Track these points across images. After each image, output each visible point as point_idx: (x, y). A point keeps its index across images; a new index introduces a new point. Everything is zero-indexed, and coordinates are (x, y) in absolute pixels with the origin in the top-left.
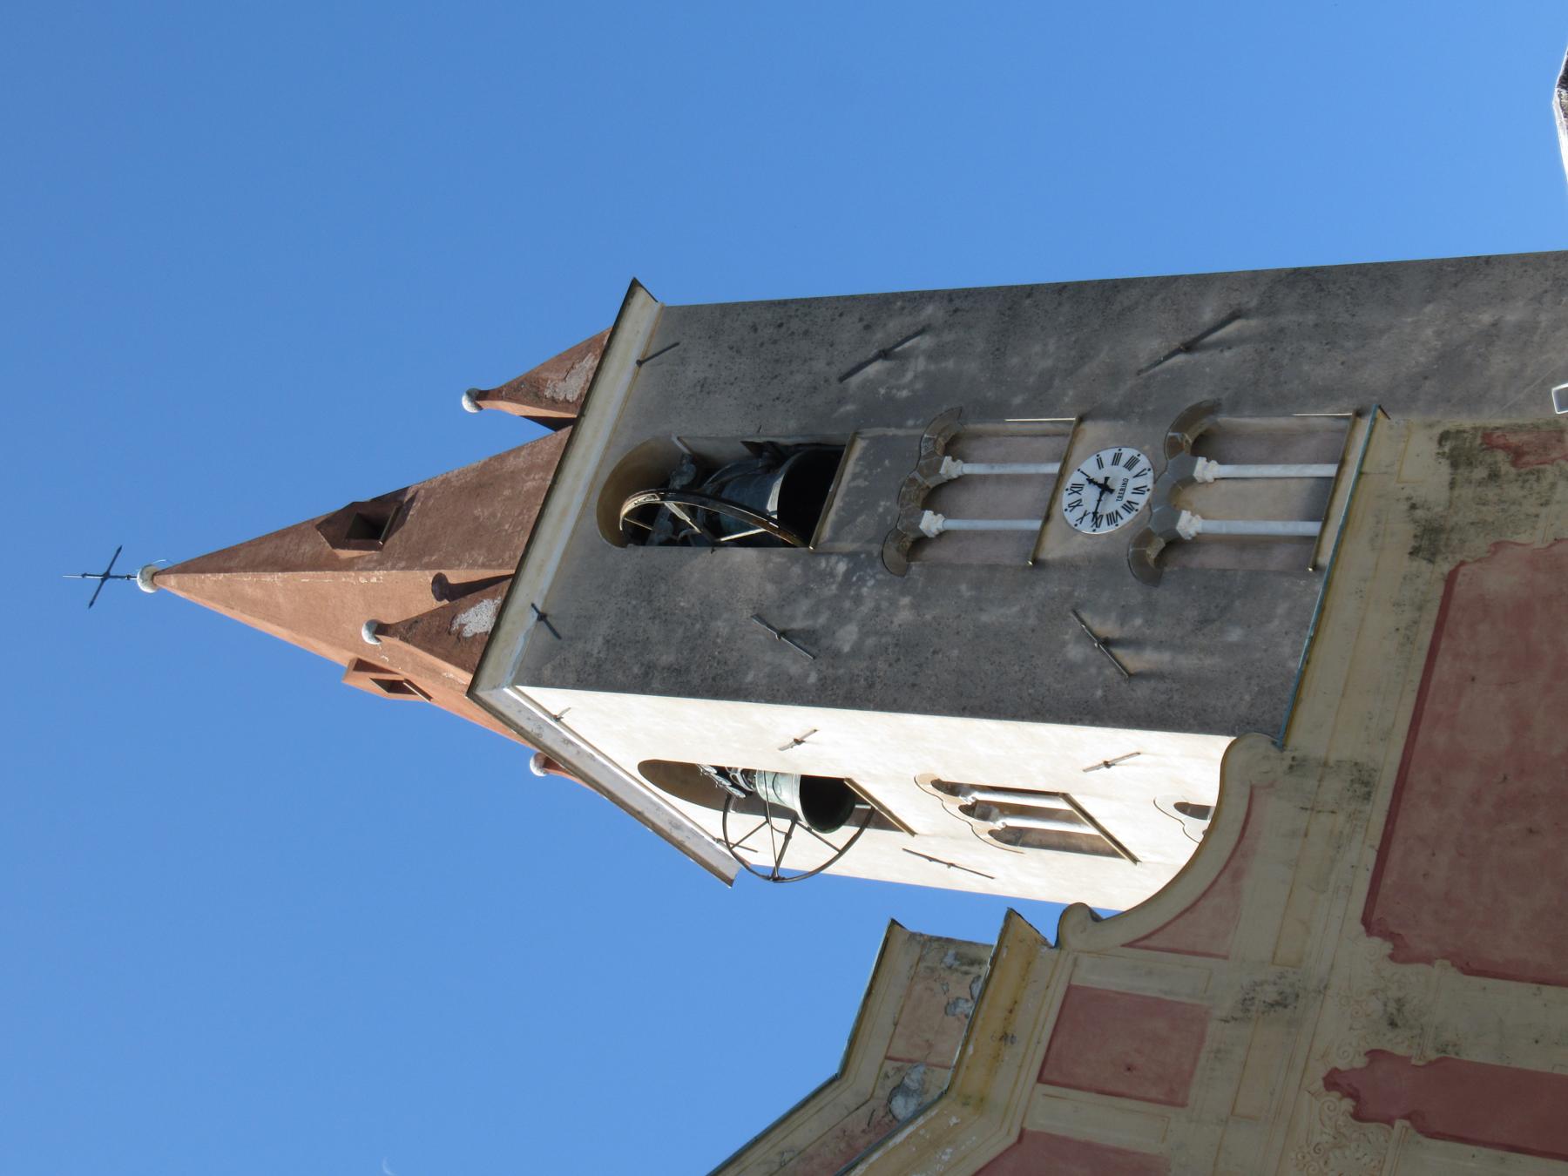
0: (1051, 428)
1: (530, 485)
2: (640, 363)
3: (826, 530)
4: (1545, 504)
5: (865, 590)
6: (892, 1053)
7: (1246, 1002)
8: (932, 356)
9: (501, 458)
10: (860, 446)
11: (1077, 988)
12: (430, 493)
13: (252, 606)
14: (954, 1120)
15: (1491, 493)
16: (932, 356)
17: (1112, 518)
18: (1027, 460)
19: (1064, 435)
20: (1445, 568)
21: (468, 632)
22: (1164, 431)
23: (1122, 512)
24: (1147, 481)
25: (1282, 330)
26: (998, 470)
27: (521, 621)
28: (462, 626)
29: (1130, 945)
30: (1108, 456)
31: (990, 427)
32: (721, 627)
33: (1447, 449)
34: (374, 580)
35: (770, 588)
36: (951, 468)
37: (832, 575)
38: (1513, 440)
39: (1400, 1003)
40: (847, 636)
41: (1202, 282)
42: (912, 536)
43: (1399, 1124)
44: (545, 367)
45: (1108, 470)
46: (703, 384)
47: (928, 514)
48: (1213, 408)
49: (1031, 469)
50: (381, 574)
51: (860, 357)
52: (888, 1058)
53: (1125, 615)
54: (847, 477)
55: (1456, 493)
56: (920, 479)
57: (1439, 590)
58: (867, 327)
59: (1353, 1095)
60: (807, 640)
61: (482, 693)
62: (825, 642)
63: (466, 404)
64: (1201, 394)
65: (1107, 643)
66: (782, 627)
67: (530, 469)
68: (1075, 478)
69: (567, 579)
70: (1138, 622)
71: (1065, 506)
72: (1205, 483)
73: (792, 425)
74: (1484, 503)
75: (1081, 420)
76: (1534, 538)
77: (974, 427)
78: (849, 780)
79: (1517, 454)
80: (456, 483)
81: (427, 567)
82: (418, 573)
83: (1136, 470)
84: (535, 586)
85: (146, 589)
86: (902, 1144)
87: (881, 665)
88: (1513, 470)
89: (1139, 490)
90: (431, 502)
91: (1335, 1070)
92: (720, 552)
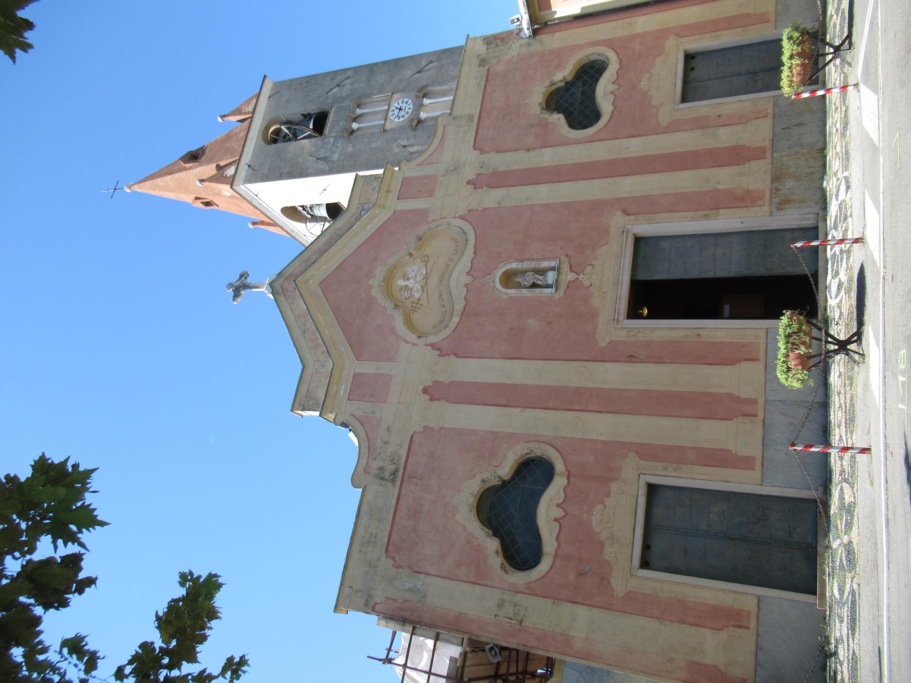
0: (384, 98)
1: (241, 135)
2: (269, 98)
3: (327, 131)
4: (510, 49)
5: (339, 145)
6: (360, 202)
7: (447, 171)
8: (351, 84)
9: (232, 131)
10: (333, 110)
11: (405, 178)
12: (212, 145)
13: (161, 188)
14: (378, 211)
15: (497, 49)
16: (351, 84)
17: (403, 116)
18: (380, 106)
19: (386, 100)
20: (487, 68)
21: (228, 175)
22: (414, 93)
23: (405, 115)
24: (411, 106)
25: (443, 65)
26: (372, 110)
27: (243, 168)
28: (226, 174)
29: (417, 165)
30: (400, 102)
31: (368, 100)
32: (301, 160)
33: (485, 41)
34: (198, 171)
35: (313, 148)
36: (359, 111)
37: (330, 142)
38: (501, 37)
39: (483, 163)
40: (335, 157)
41: (421, 56)
42: (350, 130)
43: (484, 188)
44: (242, 105)
45: (401, 104)
46: (288, 101)
47: (354, 123)
48: (427, 86)
49: (380, 109)
50: (200, 168)
51: (331, 88)
52: (359, 204)
53: (408, 139)
54: (330, 119)
55: (488, 51)
56: (351, 115)
57: (486, 73)
58: (332, 80)
59: (474, 184)
60: (325, 159)
61: (234, 187)
62: (329, 159)
63: (220, 120)
64: (424, 83)
65: (404, 146)
66: (317, 157)
67: (240, 132)
68: (392, 108)
69: (255, 156)
70: (412, 140)
71: (390, 115)
72: (426, 105)
73: (314, 107)
74: (495, 52)
75: (392, 94)
76: (507, 57)
77: (364, 101)
78: (339, 202)
79: (502, 40)
80: (219, 140)
81: (214, 163)
82: (211, 165)
83: (408, 104)
84: (247, 158)
85: (128, 191)
86: (365, 219)
87: (345, 162)
88: (502, 43)
89: (409, 109)
90: (212, 147)
91: (469, 180)
92: (298, 142)
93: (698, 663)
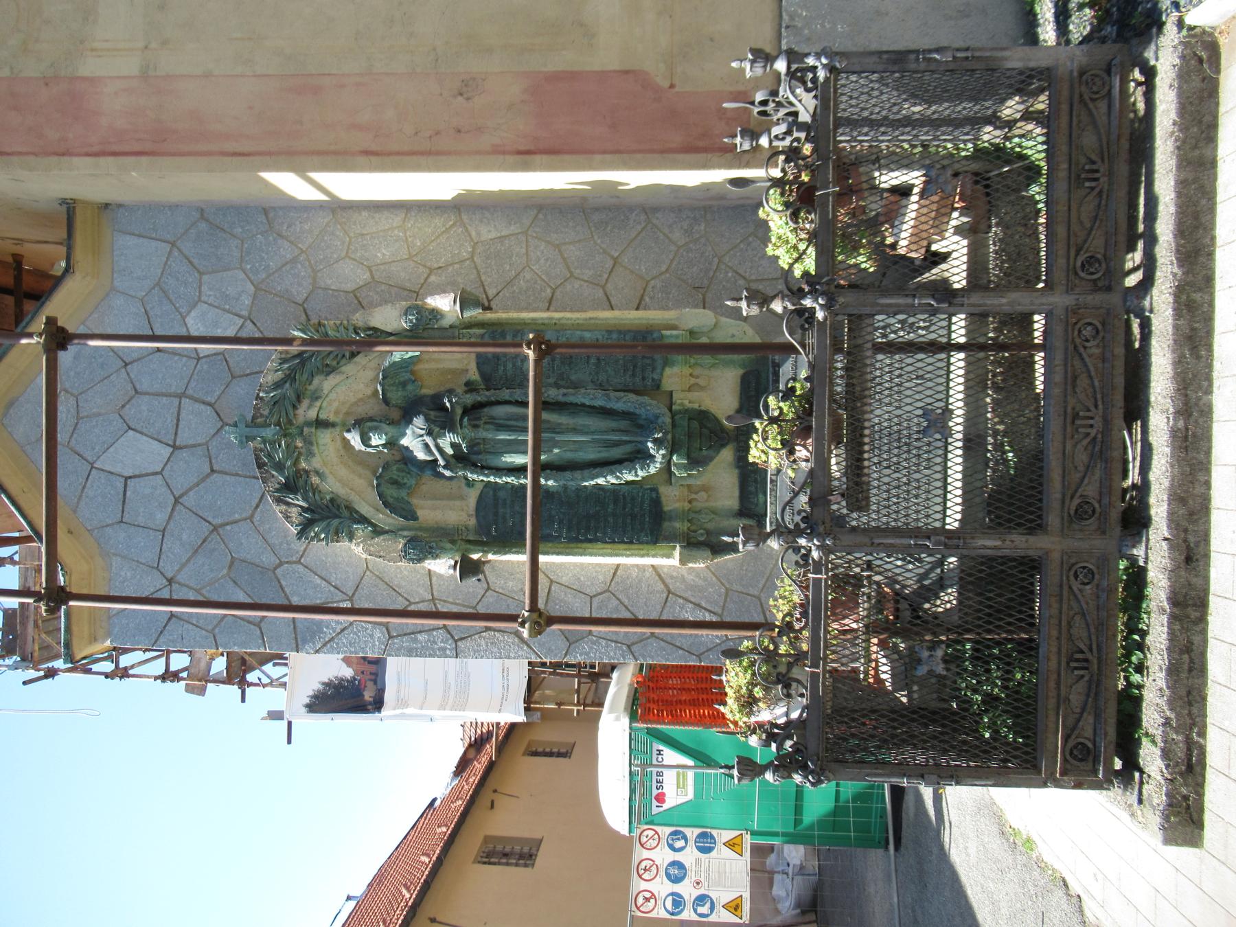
93: (572, 76)
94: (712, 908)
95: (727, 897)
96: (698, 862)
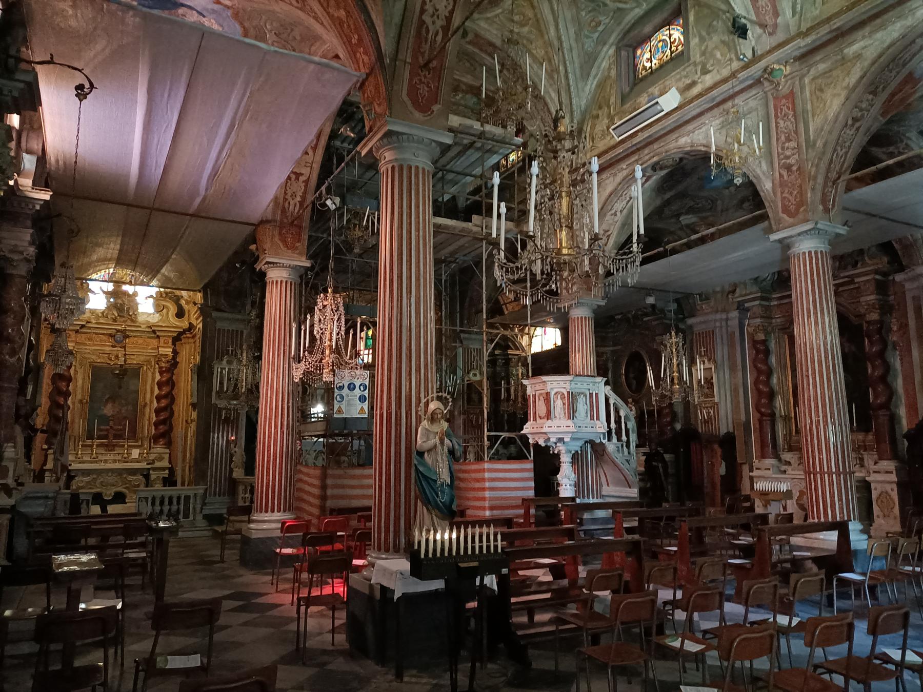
94: (339, 401)
95: (343, 407)
96: (356, 396)
